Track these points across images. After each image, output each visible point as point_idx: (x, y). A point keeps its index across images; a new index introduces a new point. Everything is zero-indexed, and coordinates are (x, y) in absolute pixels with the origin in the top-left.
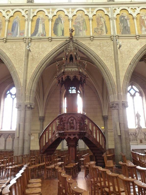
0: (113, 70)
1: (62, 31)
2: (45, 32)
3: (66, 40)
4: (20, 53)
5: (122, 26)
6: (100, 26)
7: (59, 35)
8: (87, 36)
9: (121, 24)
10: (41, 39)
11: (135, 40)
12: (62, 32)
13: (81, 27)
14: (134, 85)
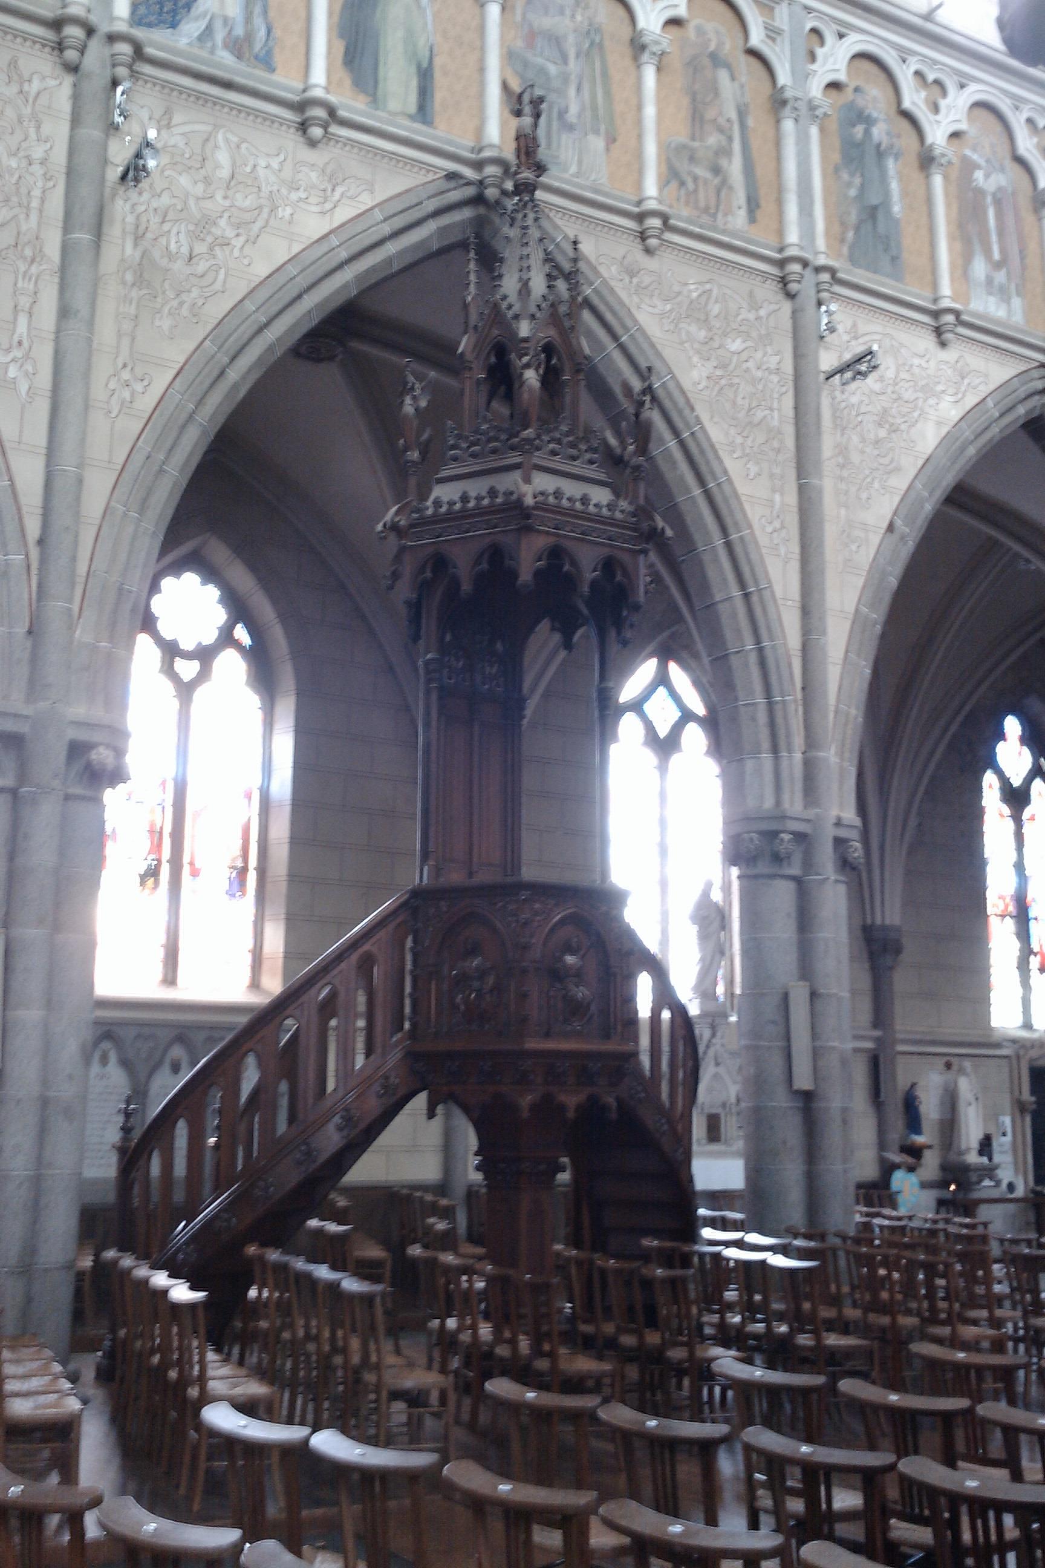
0: (783, 551)
1: (413, 69)
2: (269, 32)
3: (451, 176)
4: (13, 163)
5: (853, 192)
6: (713, 140)
7: (394, 105)
8: (615, 198)
9: (845, 176)
10: (228, 85)
11: (926, 342)
12: (414, 83)
13: (572, 92)
14: (684, 654)
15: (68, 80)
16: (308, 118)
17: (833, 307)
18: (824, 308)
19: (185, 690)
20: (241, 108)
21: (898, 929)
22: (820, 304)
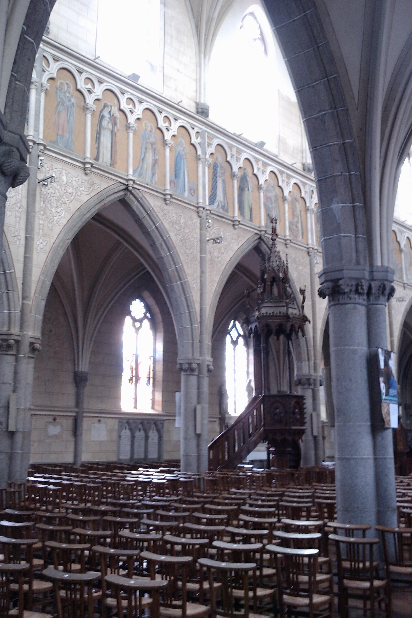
3: (256, 234)
6: (296, 219)
15: (199, 219)
16: (234, 224)
17: (43, 158)
18: (40, 158)
19: (137, 329)
20: (224, 222)
21: (87, 373)
22: (315, 257)
